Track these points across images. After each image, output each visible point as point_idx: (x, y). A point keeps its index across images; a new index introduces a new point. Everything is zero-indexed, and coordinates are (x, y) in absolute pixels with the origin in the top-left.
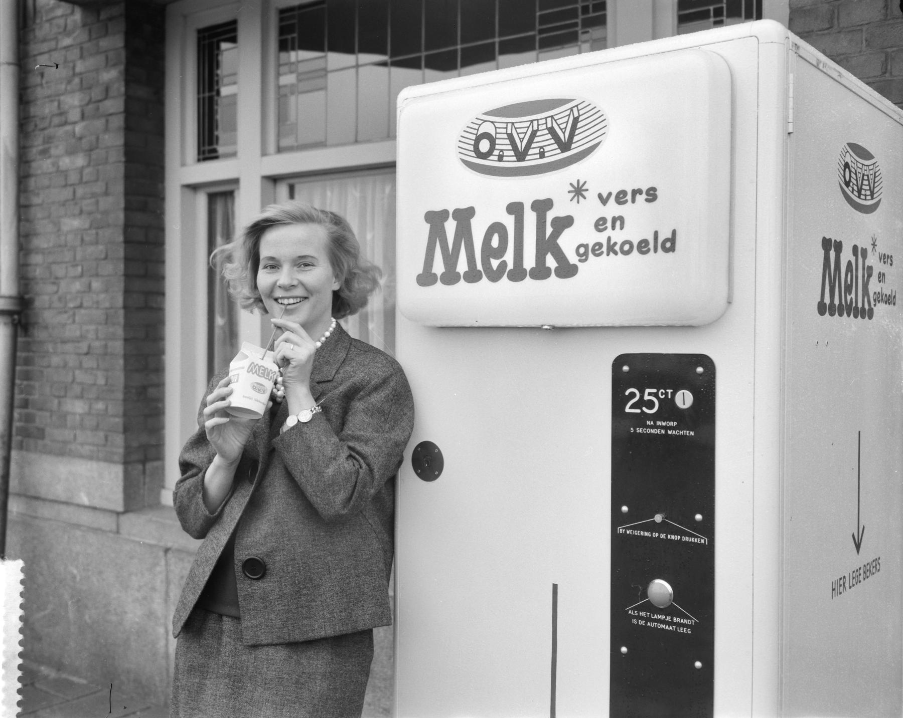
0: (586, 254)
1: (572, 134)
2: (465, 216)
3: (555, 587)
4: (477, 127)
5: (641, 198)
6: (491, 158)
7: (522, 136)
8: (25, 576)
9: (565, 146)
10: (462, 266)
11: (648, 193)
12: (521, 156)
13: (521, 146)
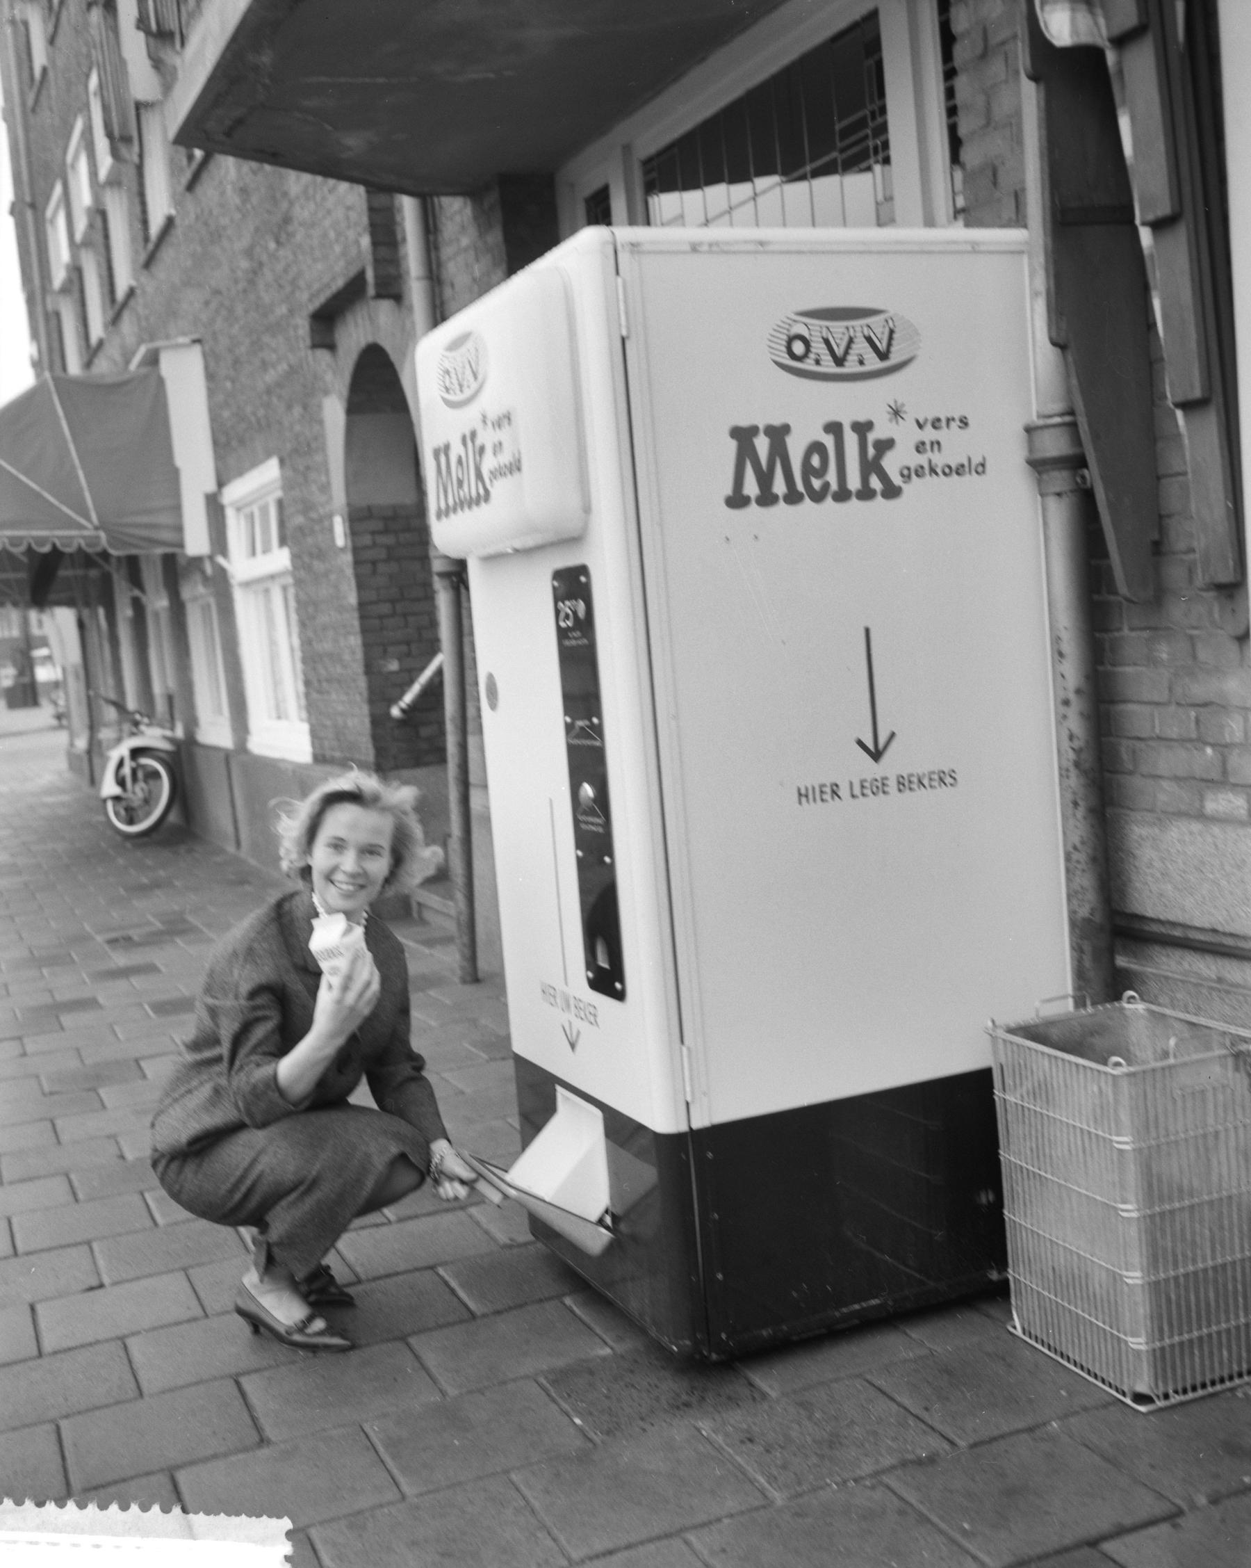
0: (909, 477)
1: (889, 345)
2: (778, 434)
3: (867, 631)
4: (787, 326)
5: (954, 425)
6: (808, 361)
8: (294, 1552)
9: (883, 356)
10: (779, 487)
11: (961, 421)
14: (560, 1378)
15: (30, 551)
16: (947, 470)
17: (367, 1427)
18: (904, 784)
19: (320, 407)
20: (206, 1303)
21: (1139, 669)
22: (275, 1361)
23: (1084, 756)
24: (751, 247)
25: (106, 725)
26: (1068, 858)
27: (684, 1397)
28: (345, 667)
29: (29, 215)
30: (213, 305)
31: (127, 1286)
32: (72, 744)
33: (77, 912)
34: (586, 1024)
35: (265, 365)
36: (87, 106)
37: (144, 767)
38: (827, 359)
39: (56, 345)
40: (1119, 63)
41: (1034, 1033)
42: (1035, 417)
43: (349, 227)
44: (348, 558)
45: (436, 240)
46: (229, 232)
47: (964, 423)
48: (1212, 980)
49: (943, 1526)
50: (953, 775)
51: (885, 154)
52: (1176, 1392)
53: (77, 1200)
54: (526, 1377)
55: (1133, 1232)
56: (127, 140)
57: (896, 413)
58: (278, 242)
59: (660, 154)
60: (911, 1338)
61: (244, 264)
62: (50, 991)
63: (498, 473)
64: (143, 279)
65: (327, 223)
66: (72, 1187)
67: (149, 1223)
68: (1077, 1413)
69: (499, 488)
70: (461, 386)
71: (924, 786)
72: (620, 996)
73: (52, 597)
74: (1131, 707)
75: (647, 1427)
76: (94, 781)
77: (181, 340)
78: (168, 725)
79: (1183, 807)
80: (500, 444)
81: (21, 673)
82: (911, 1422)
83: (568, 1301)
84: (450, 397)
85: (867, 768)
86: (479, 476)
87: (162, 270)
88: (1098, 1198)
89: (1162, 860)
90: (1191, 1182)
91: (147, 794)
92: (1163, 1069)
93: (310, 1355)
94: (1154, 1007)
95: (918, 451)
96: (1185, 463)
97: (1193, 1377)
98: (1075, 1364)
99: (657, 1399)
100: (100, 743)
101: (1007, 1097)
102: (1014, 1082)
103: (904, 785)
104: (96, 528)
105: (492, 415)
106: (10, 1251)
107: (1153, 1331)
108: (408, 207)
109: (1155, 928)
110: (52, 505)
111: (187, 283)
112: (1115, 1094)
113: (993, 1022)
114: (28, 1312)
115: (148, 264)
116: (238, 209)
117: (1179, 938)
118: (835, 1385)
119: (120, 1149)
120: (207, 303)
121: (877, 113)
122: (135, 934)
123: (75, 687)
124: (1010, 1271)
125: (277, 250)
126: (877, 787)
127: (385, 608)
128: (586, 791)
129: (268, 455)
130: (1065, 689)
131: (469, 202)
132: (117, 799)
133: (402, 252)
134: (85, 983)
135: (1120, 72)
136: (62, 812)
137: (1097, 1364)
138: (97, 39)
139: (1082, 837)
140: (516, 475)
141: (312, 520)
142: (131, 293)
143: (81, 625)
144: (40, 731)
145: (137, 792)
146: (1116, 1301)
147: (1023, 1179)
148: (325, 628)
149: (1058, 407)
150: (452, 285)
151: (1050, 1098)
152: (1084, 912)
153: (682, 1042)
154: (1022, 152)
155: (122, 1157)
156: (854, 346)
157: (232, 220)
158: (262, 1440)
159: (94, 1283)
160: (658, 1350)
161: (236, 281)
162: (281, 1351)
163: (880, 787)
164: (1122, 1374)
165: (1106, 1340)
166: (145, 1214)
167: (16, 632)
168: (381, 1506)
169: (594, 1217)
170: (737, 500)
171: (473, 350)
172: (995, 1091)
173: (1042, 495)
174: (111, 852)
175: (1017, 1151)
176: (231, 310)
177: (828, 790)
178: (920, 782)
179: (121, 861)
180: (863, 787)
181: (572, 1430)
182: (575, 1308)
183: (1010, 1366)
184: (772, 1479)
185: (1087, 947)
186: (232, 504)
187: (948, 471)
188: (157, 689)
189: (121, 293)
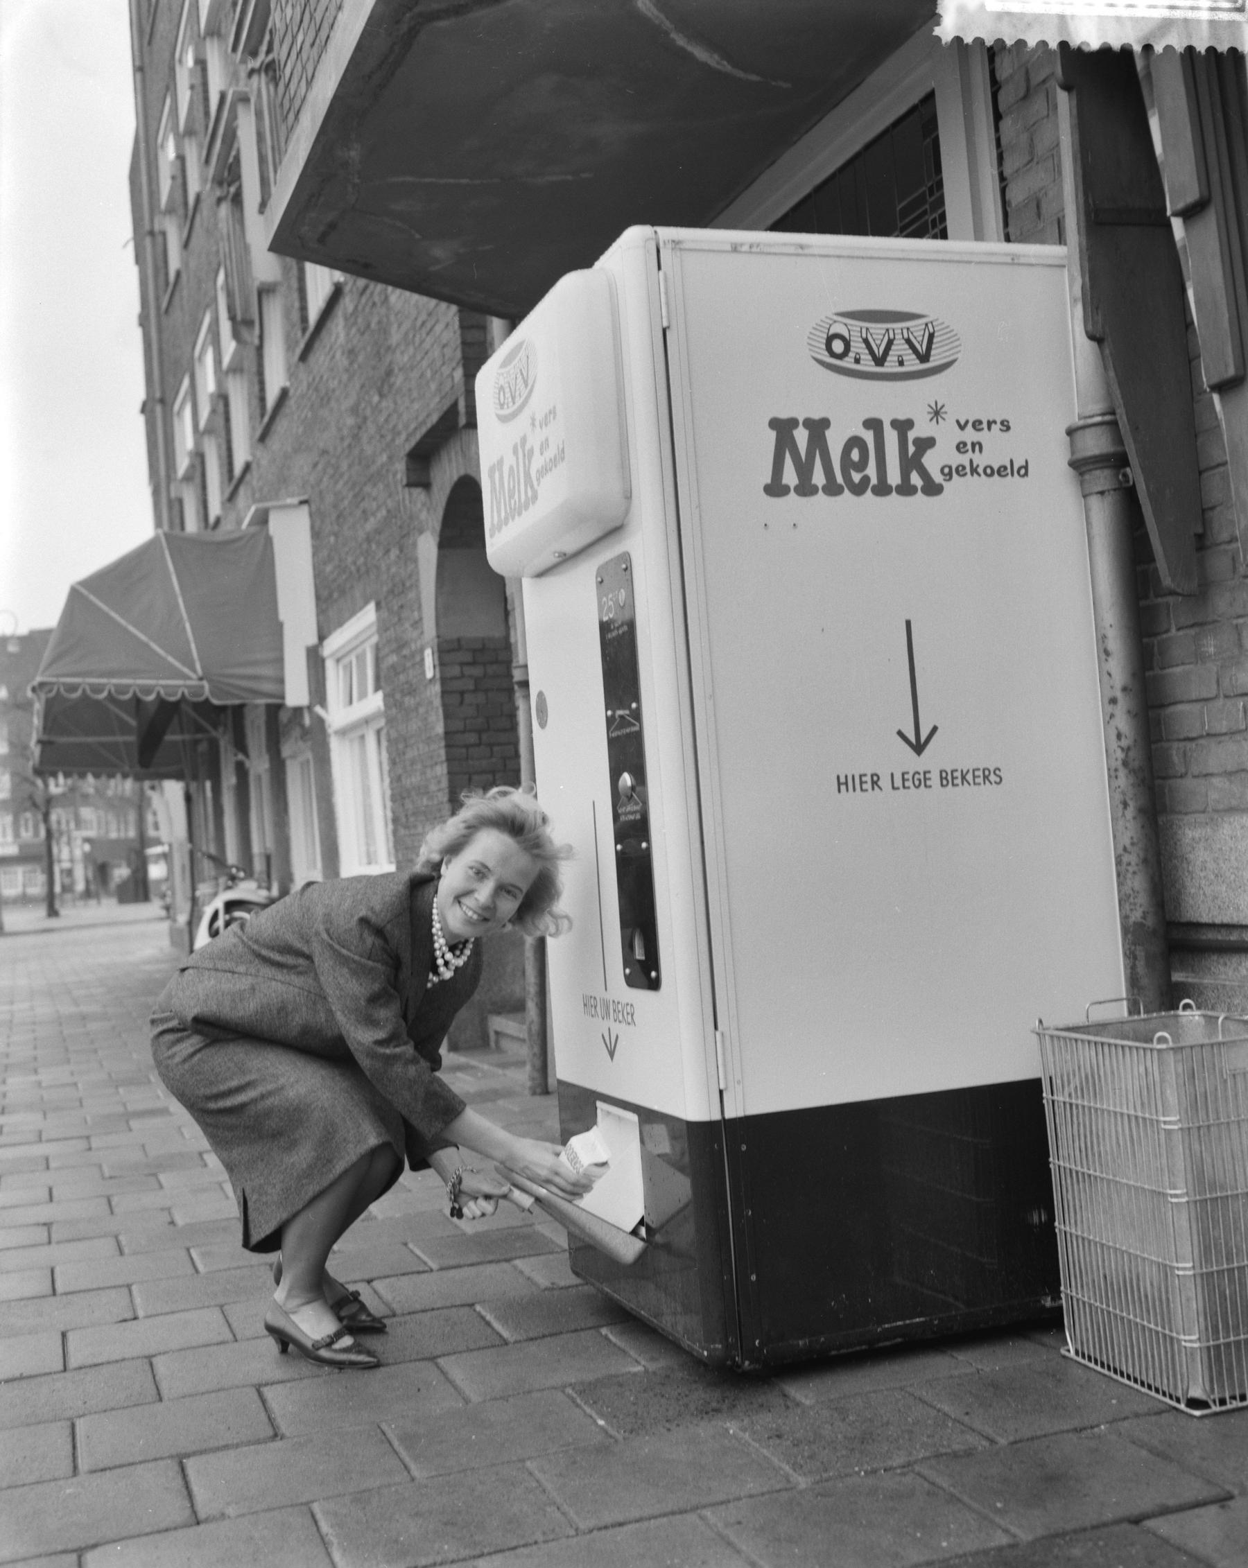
0: (950, 474)
2: (818, 428)
3: (908, 623)
6: (846, 359)
7: (878, 342)
9: (924, 358)
10: (819, 478)
11: (1002, 423)
12: (880, 361)
14: (588, 1390)
16: (989, 471)
17: (384, 1427)
18: (947, 778)
19: (415, 545)
21: (1187, 667)
22: (299, 1374)
23: (1131, 754)
24: (792, 250)
25: (204, 881)
28: (431, 798)
30: (320, 467)
31: (161, 1318)
36: (215, 299)
38: (866, 357)
44: (437, 688)
46: (337, 393)
47: (1006, 426)
49: (975, 1505)
51: (943, 226)
53: (121, 1253)
55: (1183, 1221)
56: (249, 323)
57: (937, 413)
58: (382, 395)
64: (258, 453)
65: (425, 363)
67: (190, 1271)
70: (513, 398)
72: (654, 985)
79: (1234, 803)
83: (604, 1331)
85: (913, 762)
87: (275, 442)
89: (1216, 860)
93: (337, 1371)
95: (958, 448)
98: (1129, 1378)
99: (686, 1406)
103: (946, 778)
104: (201, 679)
106: (50, 1291)
107: (1207, 1329)
109: (1211, 935)
110: (158, 655)
111: (296, 451)
113: (1041, 1022)
114: (59, 1337)
115: (263, 438)
116: (347, 370)
117: (1235, 941)
120: (315, 465)
125: (380, 402)
126: (920, 780)
127: (472, 738)
128: (626, 781)
135: (1149, 75)
138: (225, 231)
139: (1132, 838)
141: (405, 657)
142: (247, 467)
143: (188, 799)
144: (149, 921)
146: (1168, 1299)
148: (413, 763)
149: (1095, 408)
152: (1136, 916)
153: (716, 1028)
155: (172, 1223)
156: (893, 347)
158: (276, 1435)
159: (129, 1315)
161: (342, 439)
162: (306, 1368)
163: (922, 780)
167: (132, 833)
168: (389, 1485)
169: (630, 1228)
170: (775, 489)
173: (1085, 496)
176: (337, 468)
177: (868, 779)
180: (904, 780)
184: (796, 1467)
185: (1140, 953)
187: (990, 472)
188: (256, 849)
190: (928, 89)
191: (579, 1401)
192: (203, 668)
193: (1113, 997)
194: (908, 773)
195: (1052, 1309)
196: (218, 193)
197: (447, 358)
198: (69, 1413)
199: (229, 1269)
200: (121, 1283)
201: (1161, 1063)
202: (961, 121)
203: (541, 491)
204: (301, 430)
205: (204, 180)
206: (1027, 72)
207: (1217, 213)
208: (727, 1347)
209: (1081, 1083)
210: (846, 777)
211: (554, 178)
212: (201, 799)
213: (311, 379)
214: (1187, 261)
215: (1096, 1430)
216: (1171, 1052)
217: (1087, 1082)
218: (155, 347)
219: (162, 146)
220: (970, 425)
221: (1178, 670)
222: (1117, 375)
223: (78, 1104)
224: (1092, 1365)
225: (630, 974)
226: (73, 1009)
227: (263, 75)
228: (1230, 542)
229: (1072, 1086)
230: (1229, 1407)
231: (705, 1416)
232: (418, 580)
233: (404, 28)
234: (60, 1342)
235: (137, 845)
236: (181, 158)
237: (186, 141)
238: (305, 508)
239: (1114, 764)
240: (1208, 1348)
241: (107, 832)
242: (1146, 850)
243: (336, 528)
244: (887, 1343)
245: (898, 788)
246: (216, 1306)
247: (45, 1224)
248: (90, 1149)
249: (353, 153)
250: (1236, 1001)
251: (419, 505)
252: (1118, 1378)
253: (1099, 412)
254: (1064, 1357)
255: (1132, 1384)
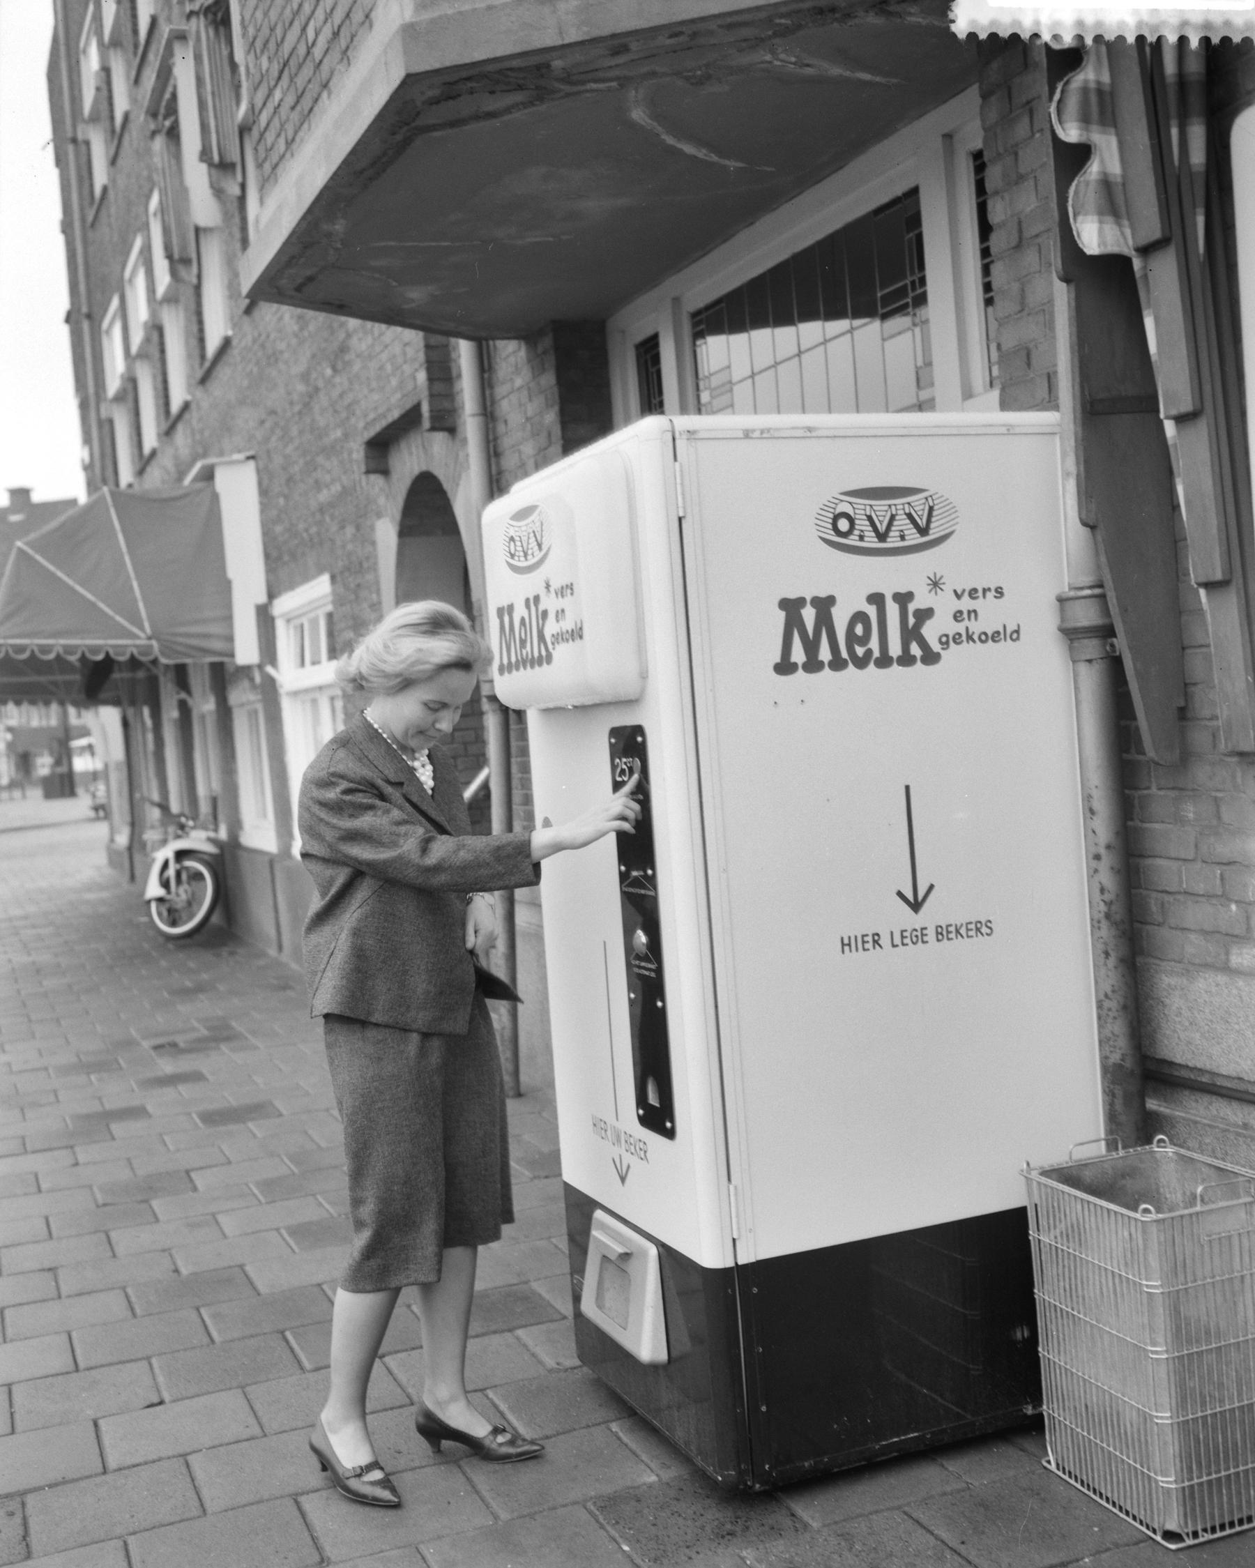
0: (947, 643)
1: (929, 521)
2: (824, 605)
3: (907, 788)
4: (833, 506)
5: (990, 595)
6: (852, 537)
9: (923, 531)
10: (825, 654)
11: (996, 591)
12: (882, 537)
13: (882, 528)
15: (83, 659)
16: (983, 637)
19: (372, 528)
20: (264, 1420)
24: (799, 433)
26: (1100, 1006)
27: (728, 1526)
29: (86, 325)
30: (268, 425)
32: (112, 840)
33: (122, 1016)
34: (635, 1158)
35: (318, 485)
36: (146, 226)
37: (187, 868)
38: (869, 535)
39: (108, 451)
40: (1145, 268)
41: (1069, 1176)
42: (1067, 589)
43: (405, 362)
45: (490, 379)
46: (286, 355)
47: (999, 592)
48: (1238, 1126)
50: (989, 924)
52: (1205, 1530)
53: (134, 1315)
54: (575, 1503)
55: (1162, 1372)
56: (186, 261)
57: (935, 584)
59: (708, 308)
60: (946, 1469)
61: (301, 387)
62: (100, 1099)
63: (559, 638)
65: (384, 356)
66: (129, 1302)
67: (206, 1340)
68: (1108, 1550)
69: (561, 652)
71: (962, 936)
72: (670, 1134)
73: (103, 696)
74: (1160, 862)
75: (694, 1555)
76: (134, 877)
77: (236, 457)
78: (212, 827)
79: (1209, 960)
80: (563, 611)
81: (58, 763)
82: (948, 1554)
83: (615, 1427)
84: (511, 561)
85: (909, 919)
86: (541, 637)
88: (1128, 1339)
89: (1190, 1009)
90: (1218, 1324)
91: (190, 896)
92: (1191, 1215)
94: (1183, 1151)
96: (1207, 634)
97: (1222, 1516)
99: (703, 1528)
100: (143, 845)
101: (1041, 1238)
102: (1048, 1223)
103: (941, 934)
104: (149, 638)
105: (555, 585)
107: (1182, 1470)
108: (464, 351)
109: (1184, 1073)
110: (106, 614)
111: (242, 402)
112: (1145, 1240)
113: (1028, 1164)
114: (92, 1429)
115: (204, 380)
116: (296, 335)
118: (874, 1517)
119: (174, 1263)
120: (262, 422)
121: (917, 284)
122: (181, 1040)
123: (117, 779)
124: (1045, 1407)
125: (333, 377)
126: (917, 936)
129: (320, 572)
130: (1096, 844)
131: (523, 344)
132: (160, 900)
133: (457, 387)
134: (133, 1091)
135: (1145, 277)
136: (102, 910)
137: (1129, 1501)
138: (160, 165)
140: (578, 641)
142: (186, 407)
143: (125, 724)
144: (76, 822)
145: (181, 895)
146: (1147, 1441)
147: (1056, 1317)
149: (1087, 580)
150: (506, 422)
151: (1083, 1239)
152: (1115, 1057)
153: (729, 1179)
154: (1054, 337)
155: (176, 1271)
156: (895, 523)
157: (289, 345)
158: (322, 1560)
159: (156, 1400)
160: (701, 1476)
161: (291, 403)
163: (919, 936)
164: (1152, 1512)
165: (1136, 1477)
166: (202, 1330)
170: (785, 667)
171: (538, 524)
172: (1031, 1232)
173: (1074, 662)
174: (154, 954)
175: (1051, 1290)
177: (869, 939)
178: (958, 931)
179: (163, 963)
180: (903, 937)
181: (619, 1556)
182: (621, 1434)
183: (1044, 1500)
185: (1119, 1091)
186: (282, 616)
187: (984, 638)
188: (201, 791)
189: (175, 407)
190: (912, 185)
191: (601, 1519)
192: (152, 626)
193: (1093, 1138)
194: (906, 931)
195: (1033, 1416)
196: (152, 126)
197: (409, 356)
198: (119, 1530)
199: (244, 1338)
200: (140, 1355)
201: (1144, 1232)
202: (948, 251)
203: (555, 654)
204: (245, 383)
205: (134, 100)
206: (1020, 223)
207: (1208, 424)
208: (740, 1473)
209: (1067, 1230)
210: (849, 938)
211: (534, 240)
212: (139, 726)
213: (256, 334)
214: (1178, 460)
215: (1081, 1563)
216: (1155, 1224)
217: (1073, 1231)
218: (80, 260)
219: (85, 52)
220: (966, 594)
221: (1157, 826)
222: (1108, 561)
223: (52, 1098)
224: (1072, 1482)
225: (644, 1115)
226: (25, 959)
227: (202, 17)
228: (1211, 719)
229: (1058, 1231)
230: (1201, 1540)
231: (721, 1541)
232: (376, 564)
233: (399, 137)
234: (94, 1435)
235: (61, 735)
236: (106, 70)
237: (112, 52)
238: (252, 464)
239: (1096, 917)
240: (1183, 1488)
241: (28, 721)
242: (1126, 998)
243: (286, 491)
244: (883, 1458)
245: (897, 946)
246: (238, 1387)
247: (50, 1269)
248: (76, 1164)
249: (337, 227)
250: (1207, 1141)
251: (377, 489)
252: (1097, 1498)
253: (1087, 585)
254: (1045, 1468)
255: (1110, 1507)
